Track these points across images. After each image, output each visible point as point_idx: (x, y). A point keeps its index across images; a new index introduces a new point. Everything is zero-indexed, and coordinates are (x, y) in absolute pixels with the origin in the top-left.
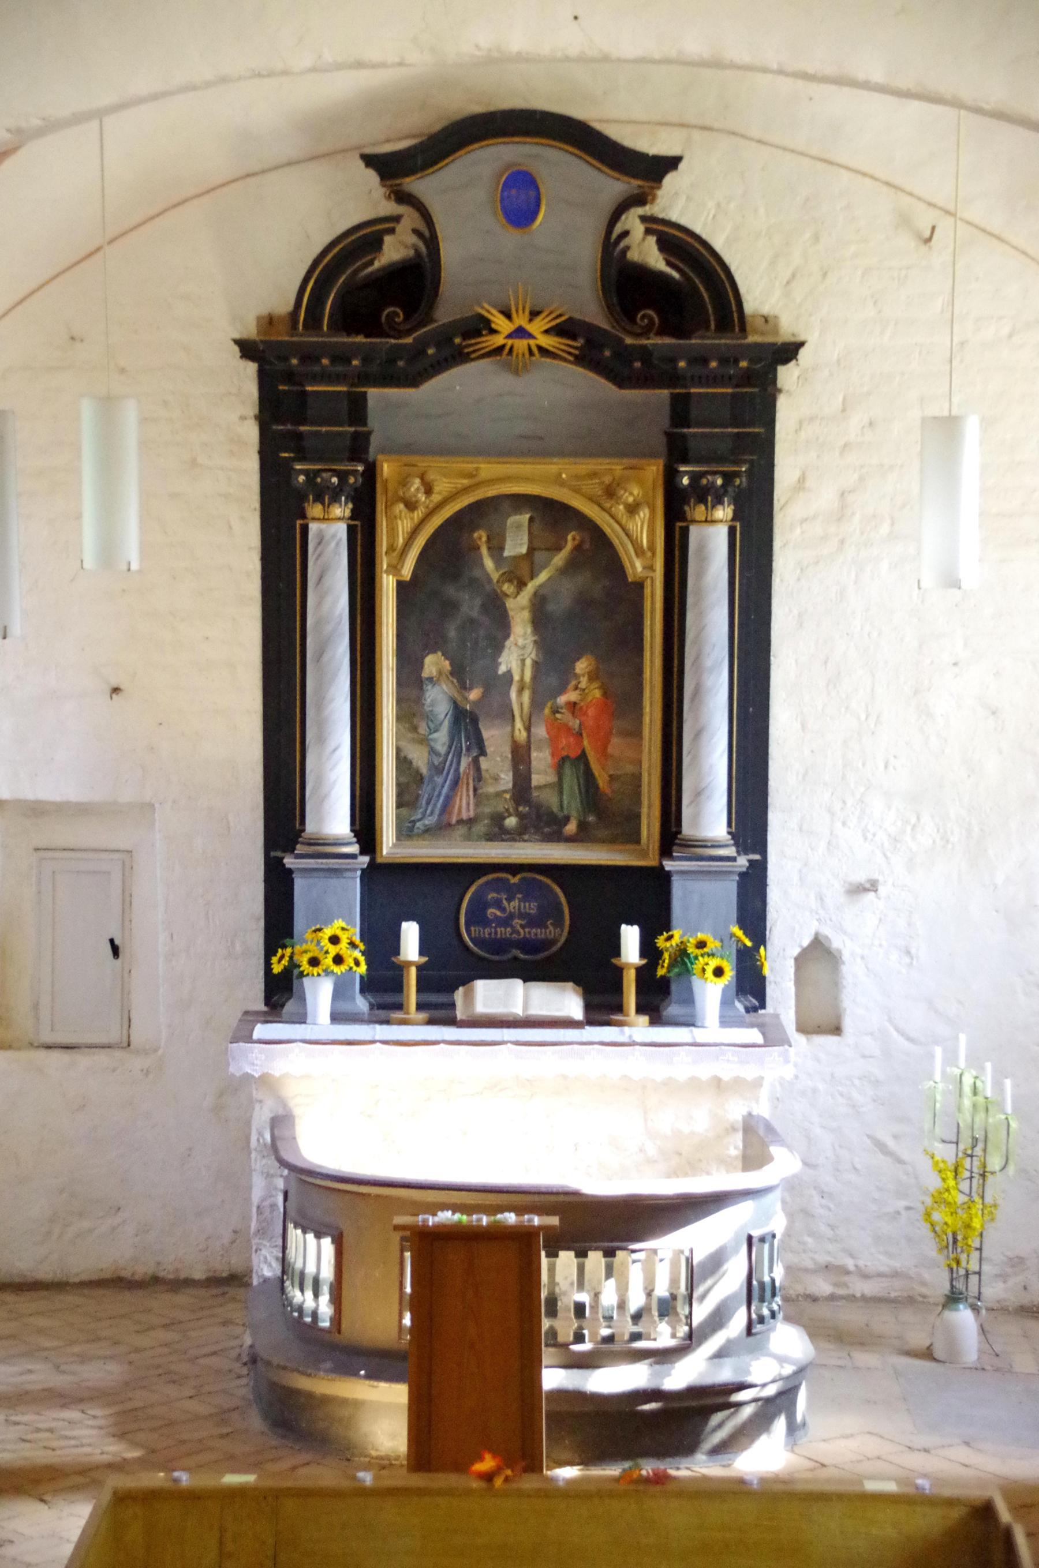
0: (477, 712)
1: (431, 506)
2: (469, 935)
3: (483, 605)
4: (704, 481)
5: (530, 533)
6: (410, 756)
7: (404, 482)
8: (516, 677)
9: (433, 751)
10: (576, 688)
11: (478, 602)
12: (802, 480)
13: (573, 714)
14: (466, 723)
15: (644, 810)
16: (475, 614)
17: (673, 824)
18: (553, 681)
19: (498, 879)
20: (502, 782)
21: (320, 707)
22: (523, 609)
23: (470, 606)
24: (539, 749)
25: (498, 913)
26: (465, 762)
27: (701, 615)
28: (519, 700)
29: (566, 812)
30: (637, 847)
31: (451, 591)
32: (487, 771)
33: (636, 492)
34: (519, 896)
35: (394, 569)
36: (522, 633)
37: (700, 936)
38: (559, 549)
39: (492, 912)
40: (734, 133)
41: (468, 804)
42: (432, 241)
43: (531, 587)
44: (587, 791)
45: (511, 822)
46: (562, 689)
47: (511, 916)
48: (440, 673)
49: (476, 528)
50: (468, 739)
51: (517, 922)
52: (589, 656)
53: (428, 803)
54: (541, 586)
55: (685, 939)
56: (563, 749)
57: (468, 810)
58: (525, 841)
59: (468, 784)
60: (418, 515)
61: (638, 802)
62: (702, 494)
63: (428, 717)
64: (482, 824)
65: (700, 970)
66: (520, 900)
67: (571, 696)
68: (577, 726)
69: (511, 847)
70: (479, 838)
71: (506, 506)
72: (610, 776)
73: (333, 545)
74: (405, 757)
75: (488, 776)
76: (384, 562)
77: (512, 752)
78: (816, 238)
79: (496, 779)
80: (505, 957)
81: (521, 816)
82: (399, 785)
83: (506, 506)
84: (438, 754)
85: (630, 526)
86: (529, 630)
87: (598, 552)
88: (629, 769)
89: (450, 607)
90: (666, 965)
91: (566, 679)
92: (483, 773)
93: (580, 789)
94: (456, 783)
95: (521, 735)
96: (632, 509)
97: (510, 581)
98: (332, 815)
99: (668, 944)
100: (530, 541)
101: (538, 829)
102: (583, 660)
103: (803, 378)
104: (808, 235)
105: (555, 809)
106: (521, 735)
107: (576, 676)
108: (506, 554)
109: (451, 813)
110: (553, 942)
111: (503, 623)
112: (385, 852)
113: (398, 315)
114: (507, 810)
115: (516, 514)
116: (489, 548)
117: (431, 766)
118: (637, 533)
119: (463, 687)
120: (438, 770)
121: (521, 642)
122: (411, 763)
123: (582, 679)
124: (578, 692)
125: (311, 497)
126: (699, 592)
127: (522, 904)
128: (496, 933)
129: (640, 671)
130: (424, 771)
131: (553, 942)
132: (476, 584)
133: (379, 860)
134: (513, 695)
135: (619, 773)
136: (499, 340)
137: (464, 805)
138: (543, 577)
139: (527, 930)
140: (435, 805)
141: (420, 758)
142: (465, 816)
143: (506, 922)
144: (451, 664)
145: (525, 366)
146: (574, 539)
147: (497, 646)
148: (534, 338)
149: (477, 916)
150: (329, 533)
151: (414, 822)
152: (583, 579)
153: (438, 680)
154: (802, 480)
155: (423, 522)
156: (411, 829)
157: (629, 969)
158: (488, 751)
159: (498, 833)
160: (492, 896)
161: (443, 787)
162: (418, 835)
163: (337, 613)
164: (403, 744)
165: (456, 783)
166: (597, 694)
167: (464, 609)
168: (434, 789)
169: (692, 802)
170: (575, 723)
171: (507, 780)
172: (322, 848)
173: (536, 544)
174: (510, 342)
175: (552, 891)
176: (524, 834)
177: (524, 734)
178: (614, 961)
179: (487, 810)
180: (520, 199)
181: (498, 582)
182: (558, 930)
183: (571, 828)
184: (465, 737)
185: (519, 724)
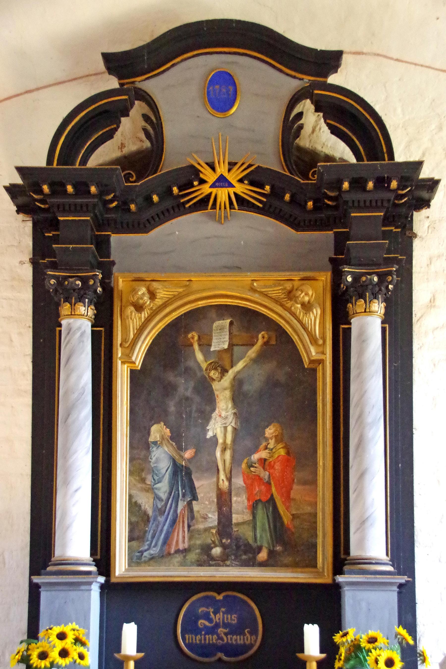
2: (184, 639)
4: (364, 279)
6: (140, 501)
7: (134, 291)
8: (220, 441)
9: (157, 497)
10: (266, 448)
11: (191, 384)
12: (433, 300)
13: (264, 468)
14: (182, 476)
15: (320, 541)
16: (189, 393)
17: (342, 552)
18: (248, 443)
19: (207, 597)
20: (210, 520)
21: (66, 459)
22: (225, 389)
23: (185, 387)
24: (238, 495)
25: (207, 624)
26: (181, 505)
27: (362, 383)
28: (223, 458)
29: (259, 543)
30: (314, 570)
31: (171, 377)
32: (198, 512)
33: (310, 293)
34: (223, 609)
35: (127, 359)
36: (224, 407)
37: (372, 633)
39: (202, 622)
40: (378, 55)
41: (184, 537)
42: (154, 127)
43: (231, 373)
44: (275, 526)
45: (217, 551)
46: (256, 450)
47: (217, 626)
48: (162, 438)
49: (192, 330)
50: (183, 487)
51: (221, 631)
53: (153, 537)
54: (238, 372)
55: (358, 637)
56: (256, 494)
57: (184, 542)
58: (227, 566)
59: (183, 522)
60: (144, 315)
61: (315, 535)
62: (361, 291)
63: (153, 471)
65: (373, 661)
66: (224, 613)
67: (263, 454)
68: (266, 477)
69: (217, 571)
70: (192, 564)
72: (293, 515)
73: (78, 334)
76: (119, 352)
78: (440, 128)
79: (205, 518)
80: (213, 659)
82: (131, 523)
83: (213, 314)
84: (160, 499)
85: (305, 320)
86: (230, 405)
87: (282, 346)
88: (308, 509)
89: (169, 389)
90: (342, 658)
91: (258, 439)
92: (196, 514)
93: (269, 527)
94: (174, 522)
95: (224, 485)
96: (307, 307)
97: (216, 369)
98: (75, 541)
99: (344, 639)
100: (230, 339)
101: (237, 557)
102: (271, 427)
103: (432, 228)
104: (433, 127)
105: (251, 541)
106: (224, 485)
108: (212, 349)
109: (170, 546)
110: (251, 646)
111: (210, 400)
112: (117, 574)
113: (132, 177)
114: (214, 542)
116: (200, 345)
118: (317, 320)
120: (161, 512)
121: (223, 414)
122: (140, 506)
123: (270, 441)
124: (267, 451)
125: (62, 300)
126: (360, 366)
127: (225, 616)
128: (205, 639)
129: (314, 435)
130: (150, 512)
131: (251, 646)
133: (113, 580)
134: (218, 454)
135: (299, 512)
136: (206, 189)
137: (181, 539)
138: (240, 365)
139: (229, 637)
140: (158, 539)
141: (146, 503)
142: (181, 547)
143: (212, 631)
144: (171, 432)
145: (226, 217)
146: (263, 337)
147: (206, 417)
148: (233, 186)
149: (191, 626)
150: (78, 325)
151: (142, 552)
152: (269, 367)
154: (433, 300)
155: (148, 320)
156: (140, 558)
157: (311, 662)
159: (206, 559)
160: (201, 610)
162: (145, 562)
163: (81, 385)
164: (134, 492)
165: (174, 522)
166: (282, 452)
168: (157, 526)
169: (358, 529)
170: (265, 475)
171: (213, 518)
172: (71, 575)
173: (235, 341)
174: (214, 190)
175: (249, 606)
176: (227, 560)
177: (226, 483)
178: (300, 655)
179: (198, 542)
180: (222, 94)
181: (206, 370)
182: (254, 637)
183: (263, 555)
184: (181, 485)
185: (222, 476)
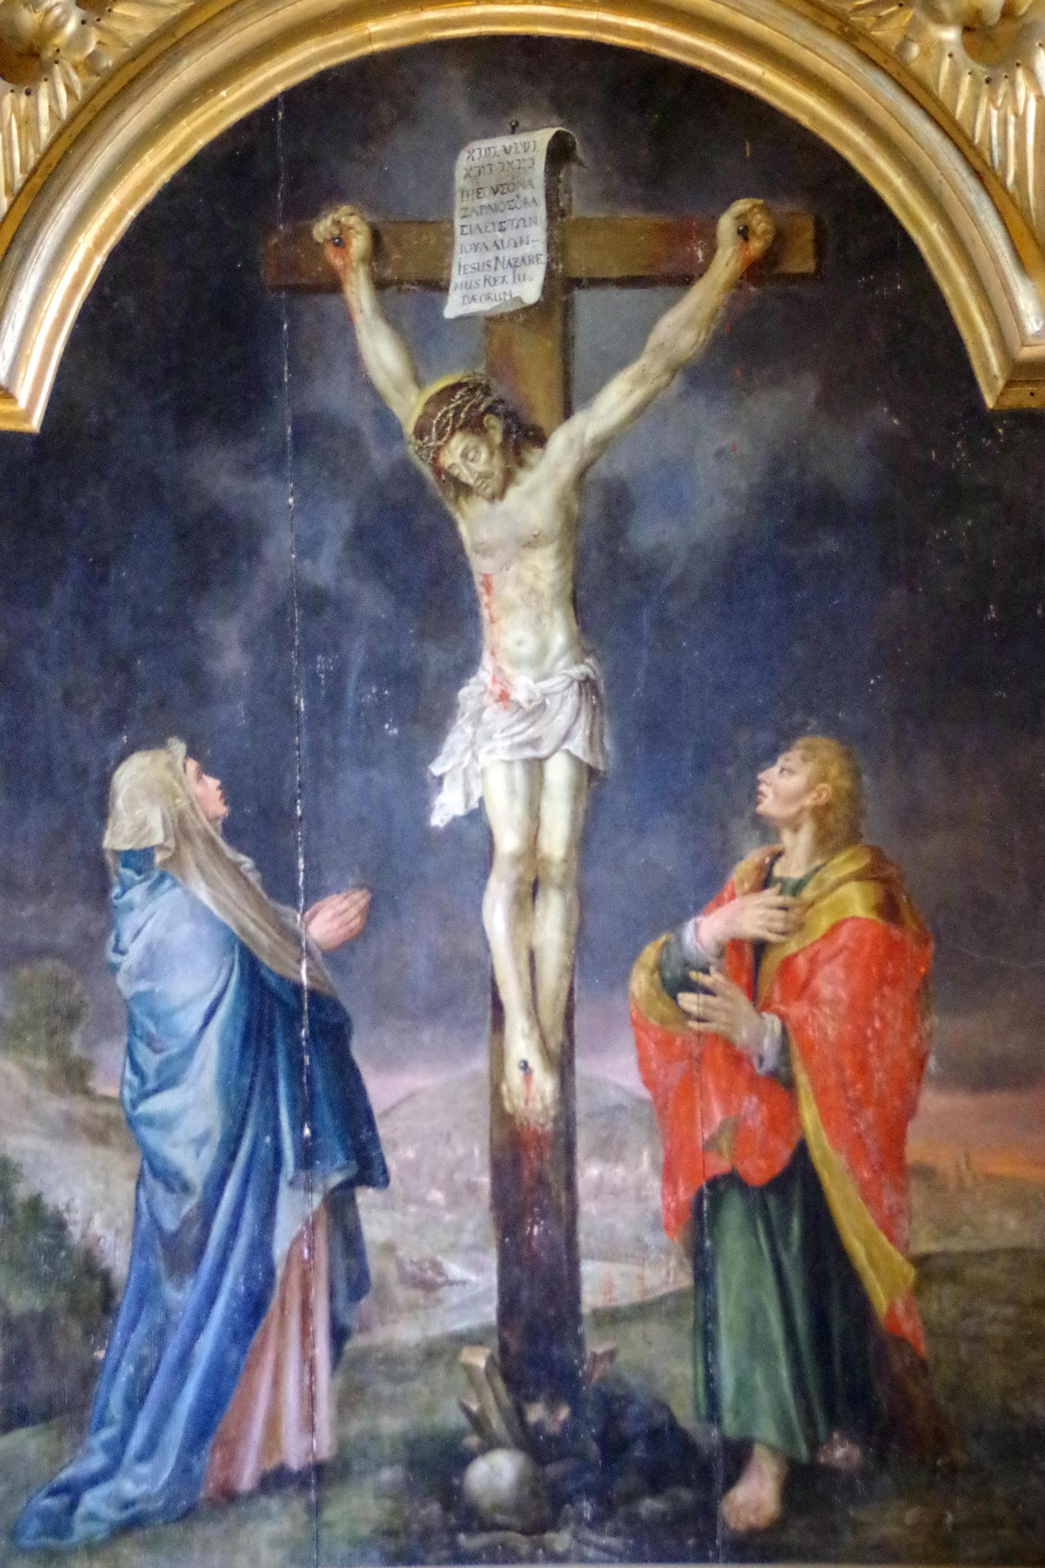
0: (349, 1004)
1: (108, 62)
3: (360, 536)
5: (555, 212)
6: (56, 1198)
8: (508, 841)
9: (156, 1171)
10: (765, 880)
11: (338, 518)
13: (752, 992)
14: (296, 1045)
16: (323, 571)
20: (453, 1296)
22: (532, 543)
23: (301, 537)
24: (609, 1149)
26: (295, 1211)
28: (523, 939)
29: (730, 1425)
31: (218, 474)
32: (389, 1248)
36: (529, 648)
38: (684, 280)
41: (310, 1399)
45: (496, 1473)
46: (708, 888)
48: (180, 829)
52: (826, 748)
53: (134, 1404)
54: (604, 444)
56: (711, 1144)
57: (309, 1425)
59: (306, 1311)
63: (135, 1023)
64: (369, 1482)
67: (747, 915)
68: (769, 1046)
71: (452, 95)
72: (921, 1262)
74: (35, 1204)
75: (392, 1274)
77: (498, 1169)
79: (428, 1284)
81: (534, 1445)
83: (452, 95)
84: (172, 1181)
86: (559, 634)
89: (213, 548)
92: (375, 1263)
94: (254, 1308)
95: (533, 1092)
97: (475, 426)
102: (791, 758)
105: (686, 1414)
106: (533, 1092)
107: (766, 829)
108: (454, 307)
114: (478, 1423)
115: (487, 135)
116: (380, 285)
117: (148, 1236)
119: (282, 887)
121: (523, 686)
122: (61, 1225)
123: (787, 838)
124: (770, 896)
130: (118, 1259)
132: (317, 441)
135: (955, 1245)
138: (613, 403)
140: (166, 1410)
142: (294, 1453)
144: (230, 794)
146: (744, 233)
147: (420, 704)
152: (780, 405)
153: (175, 858)
158: (391, 1163)
161: (198, 1330)
165: (254, 1308)
166: (857, 902)
167: (280, 547)
168: (159, 1337)
170: (760, 1033)
171: (473, 1287)
176: (552, 1524)
177: (545, 1084)
179: (391, 1424)
181: (421, 432)
184: (293, 1101)
185: (521, 1044)
